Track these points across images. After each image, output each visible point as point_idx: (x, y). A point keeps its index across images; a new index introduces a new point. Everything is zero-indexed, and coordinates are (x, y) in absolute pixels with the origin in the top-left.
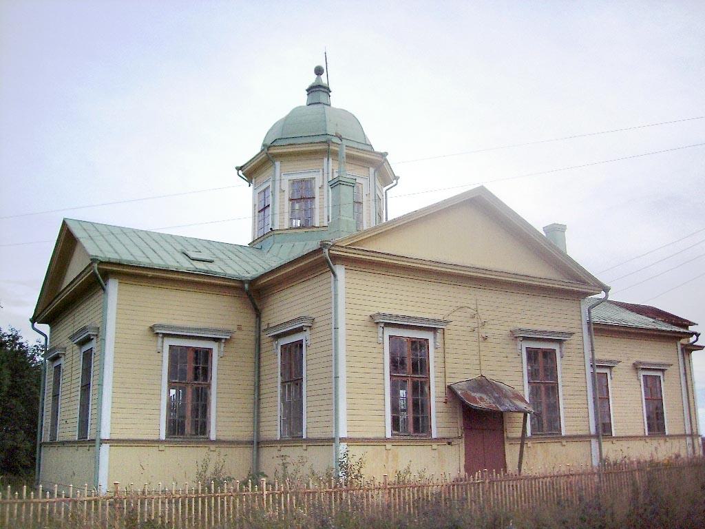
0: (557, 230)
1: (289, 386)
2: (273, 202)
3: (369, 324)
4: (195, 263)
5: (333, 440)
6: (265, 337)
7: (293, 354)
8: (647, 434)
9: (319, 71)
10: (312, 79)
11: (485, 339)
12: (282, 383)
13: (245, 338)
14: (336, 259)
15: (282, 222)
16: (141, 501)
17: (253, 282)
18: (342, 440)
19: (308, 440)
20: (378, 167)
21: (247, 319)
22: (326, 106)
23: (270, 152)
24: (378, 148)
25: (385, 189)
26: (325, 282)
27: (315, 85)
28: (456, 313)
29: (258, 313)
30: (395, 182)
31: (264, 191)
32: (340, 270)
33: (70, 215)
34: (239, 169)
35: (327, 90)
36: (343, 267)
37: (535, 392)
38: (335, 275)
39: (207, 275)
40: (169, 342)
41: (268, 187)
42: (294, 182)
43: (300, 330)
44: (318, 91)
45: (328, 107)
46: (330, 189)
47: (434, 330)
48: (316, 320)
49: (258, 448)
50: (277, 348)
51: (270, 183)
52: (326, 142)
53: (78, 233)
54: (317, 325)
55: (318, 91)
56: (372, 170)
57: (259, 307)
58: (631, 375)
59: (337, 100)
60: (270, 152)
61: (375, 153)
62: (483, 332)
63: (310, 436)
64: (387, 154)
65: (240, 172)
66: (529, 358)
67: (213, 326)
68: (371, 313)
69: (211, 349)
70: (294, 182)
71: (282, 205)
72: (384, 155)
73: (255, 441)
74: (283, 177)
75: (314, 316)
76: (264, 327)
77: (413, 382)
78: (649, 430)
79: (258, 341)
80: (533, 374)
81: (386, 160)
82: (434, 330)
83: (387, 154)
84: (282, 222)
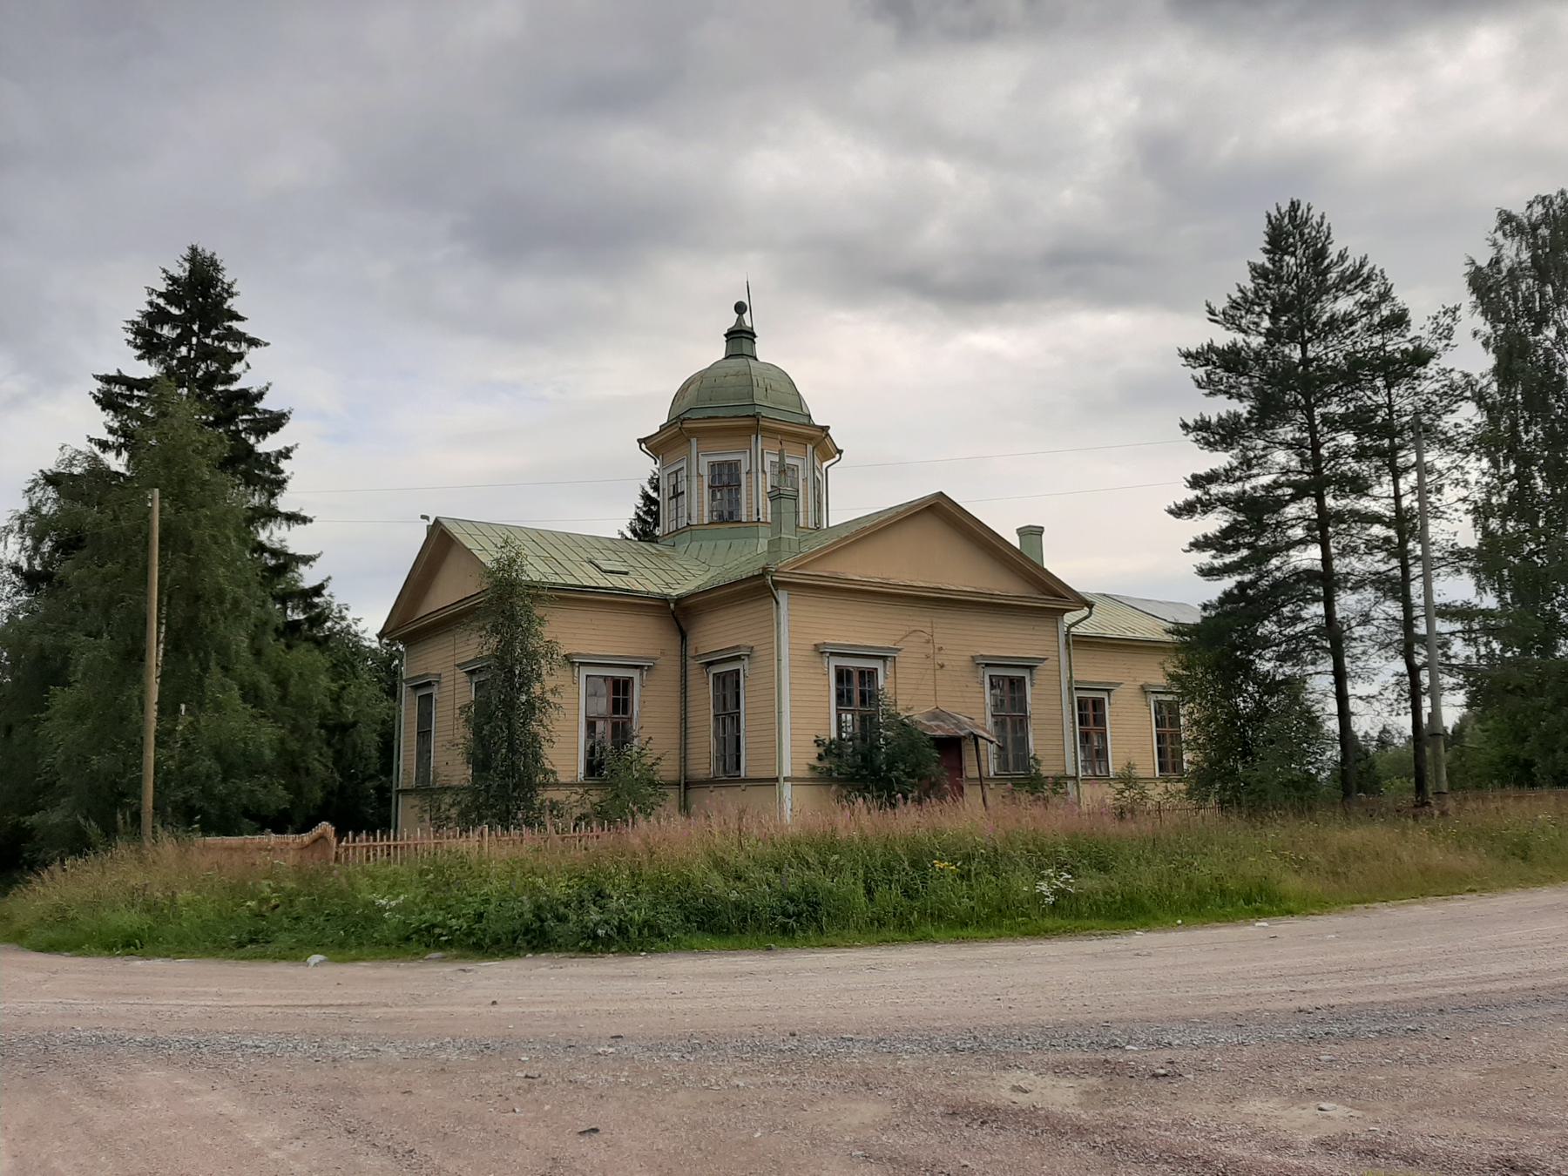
0: (1032, 534)
1: (724, 720)
2: (689, 488)
3: (813, 653)
4: (611, 577)
5: (777, 780)
6: (693, 665)
7: (729, 688)
8: (1157, 775)
9: (740, 308)
10: (731, 320)
11: (942, 666)
12: (715, 716)
13: (669, 669)
14: (777, 584)
15: (701, 515)
16: (1287, 625)
17: (679, 600)
18: (786, 779)
19: (745, 780)
20: (819, 442)
21: (673, 644)
22: (750, 360)
23: (684, 426)
24: (818, 420)
25: (825, 464)
26: (766, 607)
27: (736, 329)
28: (909, 638)
29: (684, 637)
30: (838, 456)
31: (676, 472)
32: (783, 596)
33: (449, 509)
34: (640, 441)
35: (751, 335)
36: (786, 592)
37: (999, 723)
38: (777, 603)
39: (629, 593)
40: (585, 671)
41: (682, 468)
42: (713, 465)
43: (738, 658)
44: (740, 337)
45: (751, 361)
46: (769, 502)
47: (884, 658)
48: (755, 648)
49: (685, 789)
50: (708, 677)
51: (684, 464)
52: (754, 416)
53: (456, 531)
54: (758, 653)
55: (740, 337)
56: (810, 447)
57: (684, 628)
58: (1139, 702)
59: (765, 351)
60: (684, 426)
61: (814, 426)
62: (940, 659)
63: (752, 775)
64: (828, 427)
65: (643, 446)
66: (992, 687)
67: (642, 653)
68: (816, 642)
69: (632, 678)
70: (713, 465)
71: (700, 496)
72: (825, 429)
73: (682, 782)
74: (701, 461)
75: (752, 644)
76: (691, 652)
77: (861, 717)
78: (1160, 770)
79: (684, 666)
80: (998, 705)
81: (828, 435)
82: (884, 658)
83: (828, 427)
84: (701, 515)
